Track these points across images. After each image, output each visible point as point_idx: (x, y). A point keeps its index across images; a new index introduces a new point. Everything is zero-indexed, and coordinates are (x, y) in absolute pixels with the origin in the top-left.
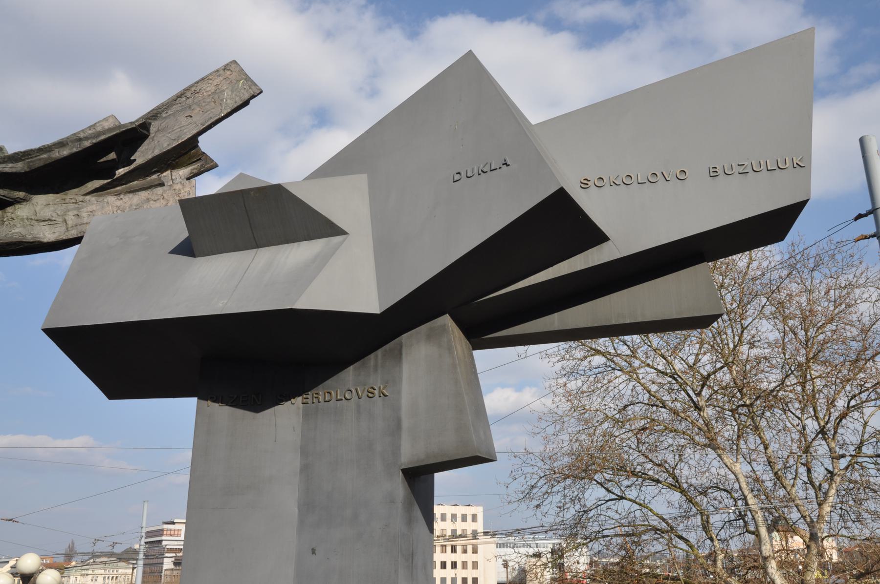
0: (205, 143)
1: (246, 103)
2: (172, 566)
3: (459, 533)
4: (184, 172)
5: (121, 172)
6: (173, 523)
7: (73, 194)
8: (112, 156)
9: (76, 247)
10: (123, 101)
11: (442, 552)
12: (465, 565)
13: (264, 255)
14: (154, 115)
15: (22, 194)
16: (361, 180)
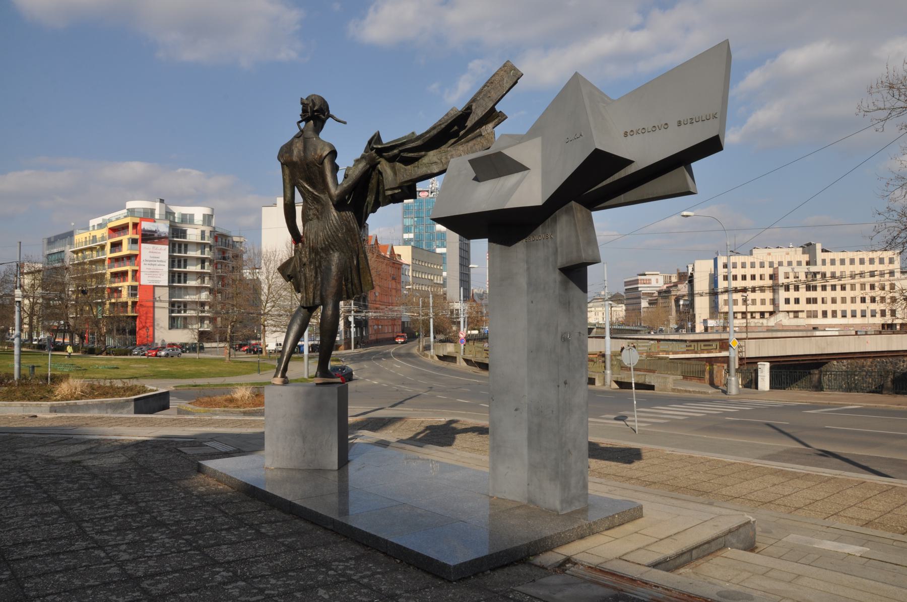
0: (498, 108)
1: (516, 82)
2: (647, 305)
3: (838, 274)
4: (490, 125)
5: (462, 133)
6: (645, 275)
7: (443, 148)
8: (456, 128)
9: (443, 176)
10: (455, 99)
11: (852, 289)
12: (863, 300)
13: (502, 180)
14: (474, 100)
15: (423, 153)
16: (538, 141)
